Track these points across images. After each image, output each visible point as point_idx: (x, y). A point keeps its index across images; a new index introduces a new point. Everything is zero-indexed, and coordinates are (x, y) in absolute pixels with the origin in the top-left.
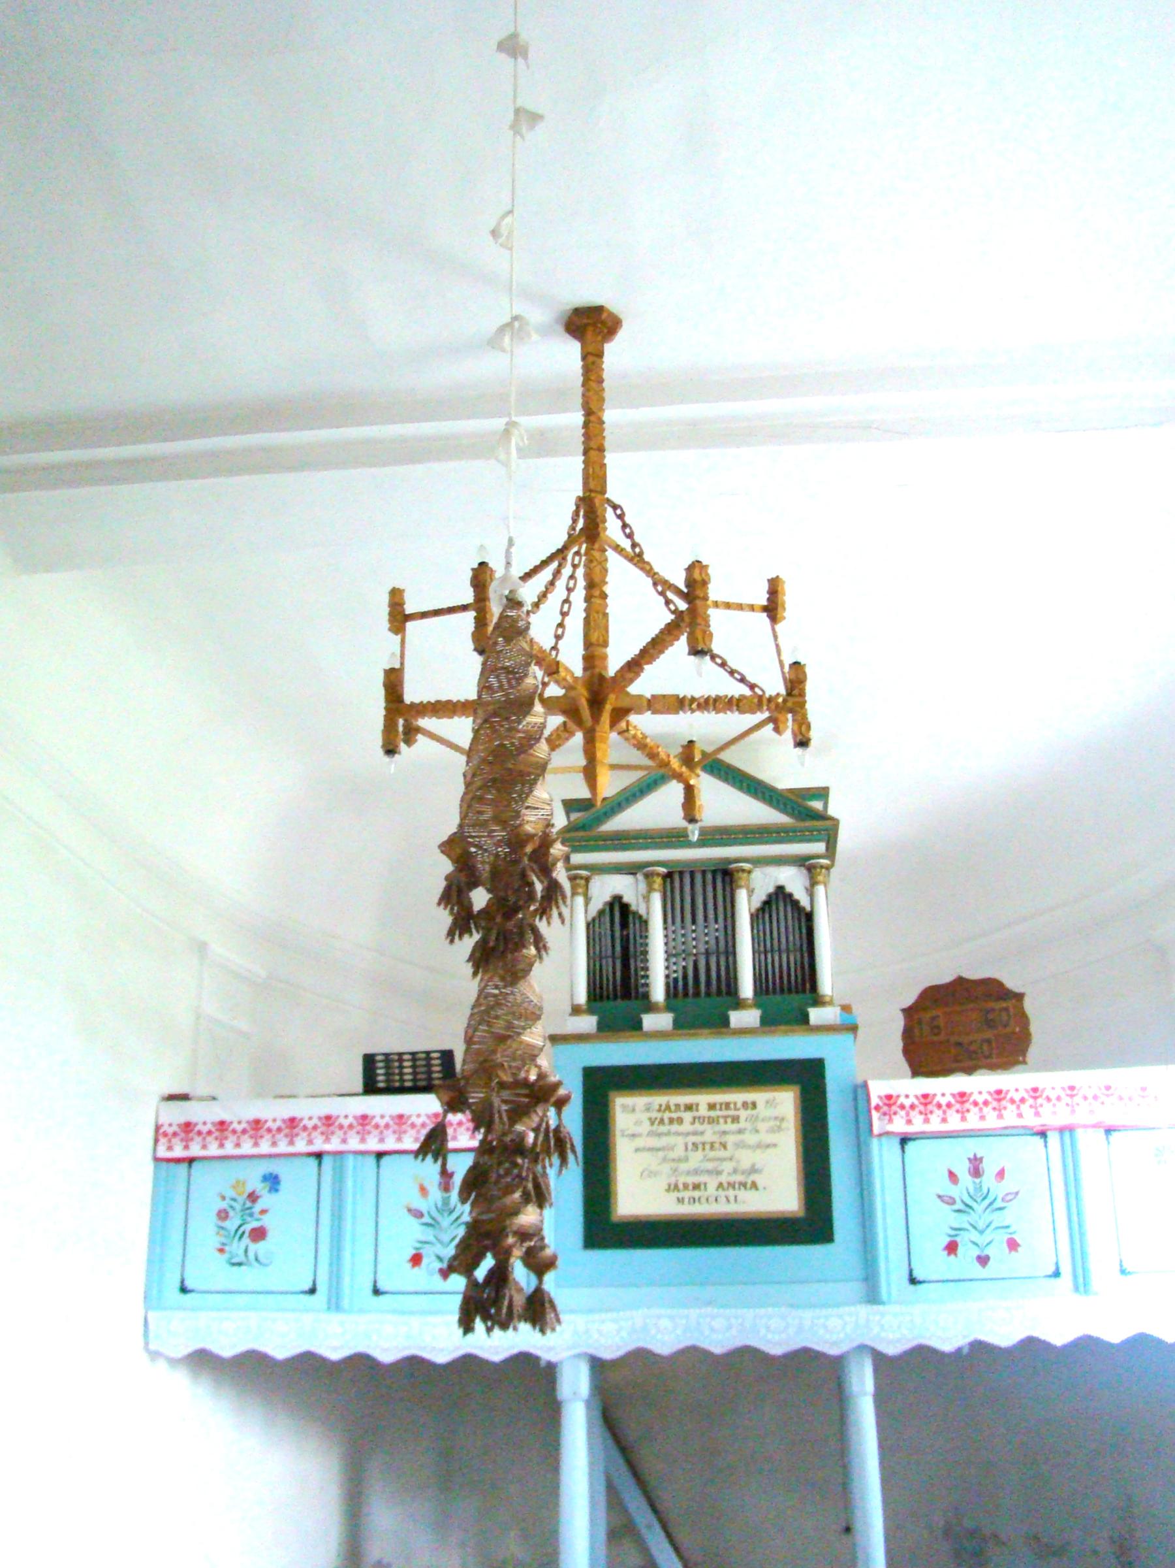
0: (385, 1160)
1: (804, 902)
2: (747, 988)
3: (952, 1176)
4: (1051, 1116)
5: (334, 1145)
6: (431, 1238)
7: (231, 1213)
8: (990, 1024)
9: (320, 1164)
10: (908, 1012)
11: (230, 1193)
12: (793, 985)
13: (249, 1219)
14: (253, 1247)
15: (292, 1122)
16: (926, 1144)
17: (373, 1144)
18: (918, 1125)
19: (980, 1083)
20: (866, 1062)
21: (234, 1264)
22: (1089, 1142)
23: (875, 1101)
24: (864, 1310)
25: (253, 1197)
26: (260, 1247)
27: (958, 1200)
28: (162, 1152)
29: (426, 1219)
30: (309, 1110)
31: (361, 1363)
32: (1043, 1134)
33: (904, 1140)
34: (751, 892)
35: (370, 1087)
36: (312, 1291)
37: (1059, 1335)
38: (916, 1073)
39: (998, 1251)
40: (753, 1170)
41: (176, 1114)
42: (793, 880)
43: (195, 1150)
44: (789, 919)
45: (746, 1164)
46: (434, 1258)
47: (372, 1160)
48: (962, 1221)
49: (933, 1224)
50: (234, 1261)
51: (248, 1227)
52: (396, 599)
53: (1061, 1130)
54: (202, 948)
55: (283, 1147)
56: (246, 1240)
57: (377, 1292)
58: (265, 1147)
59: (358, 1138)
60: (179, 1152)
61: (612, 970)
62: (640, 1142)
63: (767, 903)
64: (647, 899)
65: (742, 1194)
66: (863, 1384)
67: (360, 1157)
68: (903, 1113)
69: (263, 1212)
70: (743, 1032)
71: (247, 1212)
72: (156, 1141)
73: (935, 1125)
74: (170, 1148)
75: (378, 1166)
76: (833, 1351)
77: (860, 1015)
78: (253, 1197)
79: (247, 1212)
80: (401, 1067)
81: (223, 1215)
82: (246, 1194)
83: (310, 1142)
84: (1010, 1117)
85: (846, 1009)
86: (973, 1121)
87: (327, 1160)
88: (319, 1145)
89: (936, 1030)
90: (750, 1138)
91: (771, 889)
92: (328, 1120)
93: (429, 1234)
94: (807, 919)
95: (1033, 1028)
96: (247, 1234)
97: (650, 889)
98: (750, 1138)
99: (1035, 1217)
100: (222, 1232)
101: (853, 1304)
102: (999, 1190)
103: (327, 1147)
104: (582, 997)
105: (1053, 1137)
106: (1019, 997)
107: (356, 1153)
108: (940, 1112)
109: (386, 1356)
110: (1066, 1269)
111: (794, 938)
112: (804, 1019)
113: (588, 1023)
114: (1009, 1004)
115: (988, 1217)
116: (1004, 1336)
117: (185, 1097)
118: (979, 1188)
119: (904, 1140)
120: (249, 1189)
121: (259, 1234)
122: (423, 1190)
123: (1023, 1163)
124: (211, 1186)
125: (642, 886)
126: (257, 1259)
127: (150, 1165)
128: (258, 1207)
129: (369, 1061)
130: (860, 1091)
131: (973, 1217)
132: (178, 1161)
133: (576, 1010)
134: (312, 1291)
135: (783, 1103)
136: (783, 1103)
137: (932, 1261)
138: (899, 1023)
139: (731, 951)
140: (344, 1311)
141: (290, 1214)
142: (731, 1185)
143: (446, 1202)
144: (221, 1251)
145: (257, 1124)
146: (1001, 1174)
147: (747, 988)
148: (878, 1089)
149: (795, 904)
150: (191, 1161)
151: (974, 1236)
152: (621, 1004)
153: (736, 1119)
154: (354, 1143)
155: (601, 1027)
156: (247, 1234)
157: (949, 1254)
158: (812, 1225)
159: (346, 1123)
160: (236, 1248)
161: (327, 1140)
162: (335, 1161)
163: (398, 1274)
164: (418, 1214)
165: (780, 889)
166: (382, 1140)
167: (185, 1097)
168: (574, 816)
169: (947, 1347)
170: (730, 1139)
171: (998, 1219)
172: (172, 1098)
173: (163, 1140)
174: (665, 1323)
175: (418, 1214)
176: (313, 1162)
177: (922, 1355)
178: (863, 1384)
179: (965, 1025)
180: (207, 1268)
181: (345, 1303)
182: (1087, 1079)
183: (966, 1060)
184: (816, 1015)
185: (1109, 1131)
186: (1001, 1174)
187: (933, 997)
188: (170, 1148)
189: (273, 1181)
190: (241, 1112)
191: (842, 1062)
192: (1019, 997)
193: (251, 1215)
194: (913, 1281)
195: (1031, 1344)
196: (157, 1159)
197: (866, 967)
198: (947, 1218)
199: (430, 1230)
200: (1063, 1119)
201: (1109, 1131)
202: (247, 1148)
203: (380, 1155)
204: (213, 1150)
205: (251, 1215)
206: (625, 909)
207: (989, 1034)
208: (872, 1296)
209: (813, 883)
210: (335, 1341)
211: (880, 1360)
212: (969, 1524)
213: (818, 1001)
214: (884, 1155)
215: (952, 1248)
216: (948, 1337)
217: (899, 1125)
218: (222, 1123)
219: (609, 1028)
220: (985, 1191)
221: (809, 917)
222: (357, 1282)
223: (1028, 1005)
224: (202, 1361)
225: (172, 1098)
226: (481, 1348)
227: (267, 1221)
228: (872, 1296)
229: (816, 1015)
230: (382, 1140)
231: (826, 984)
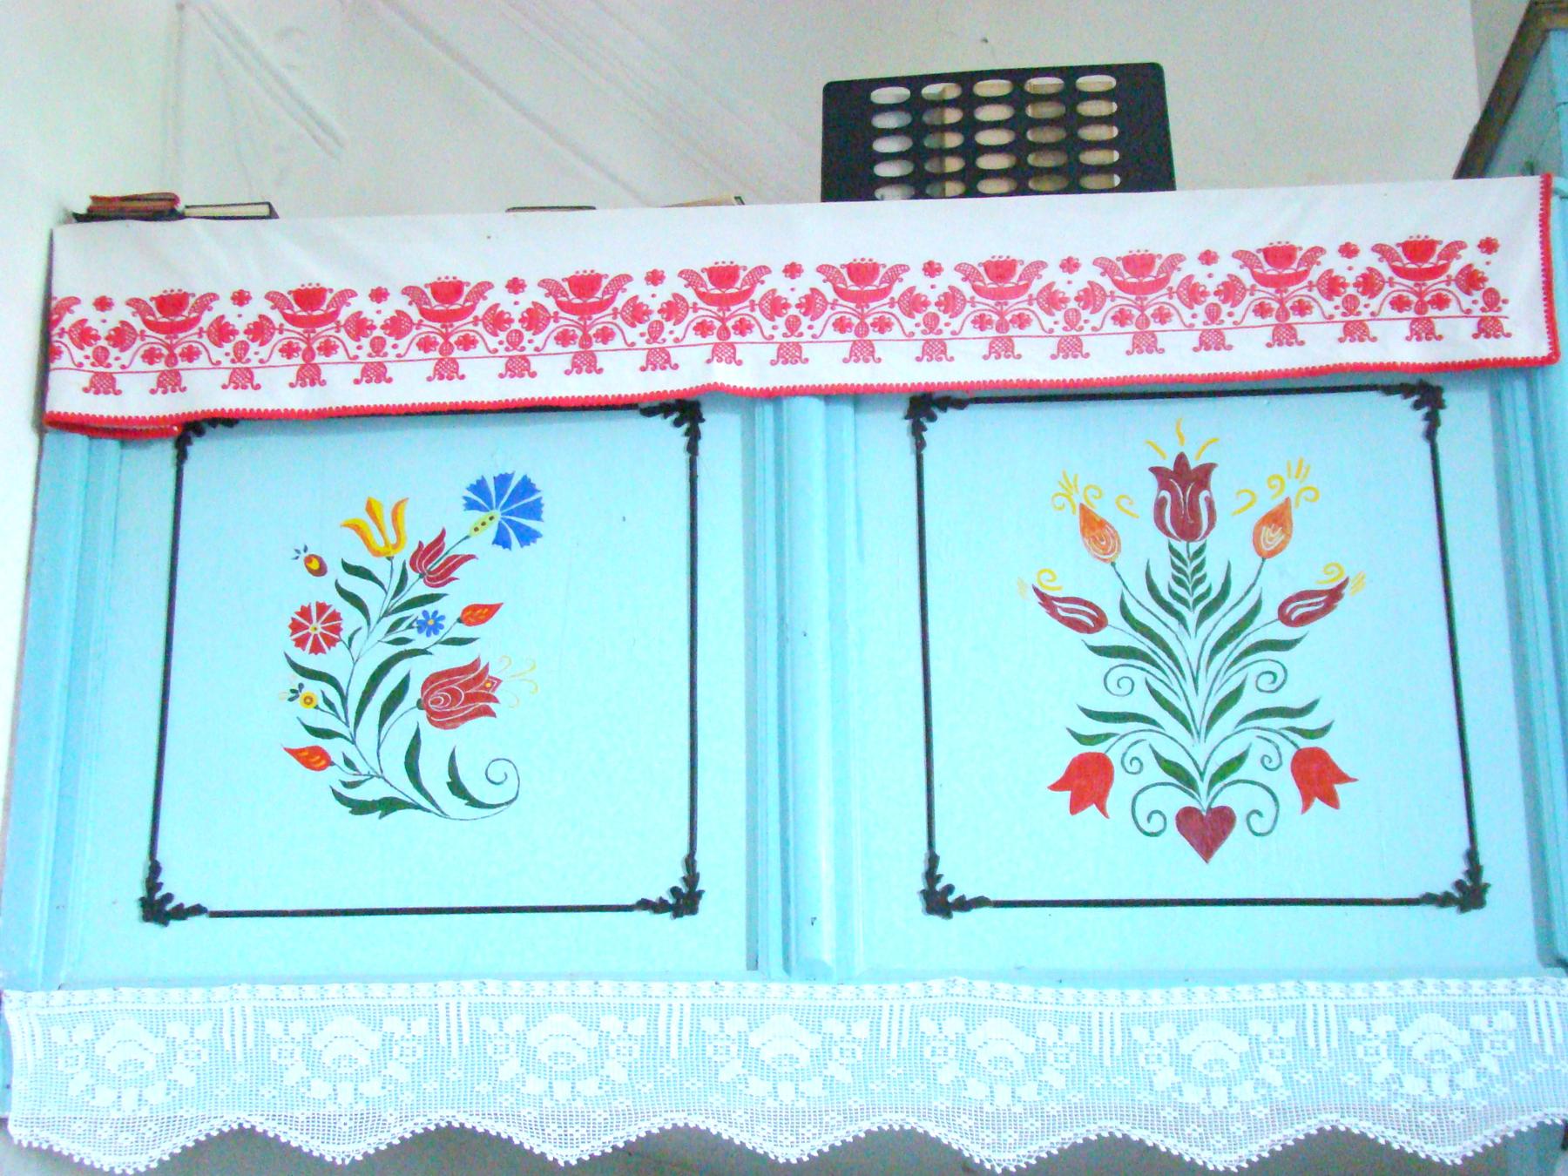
0: (944, 428)
5: (754, 367)
6: (1143, 704)
7: (351, 618)
9: (694, 437)
11: (341, 548)
13: (420, 641)
14: (437, 744)
15: (172, 309)
17: (900, 363)
21: (360, 808)
25: (437, 563)
26: (472, 742)
27: (1113, 616)
28: (70, 396)
29: (1116, 634)
30: (649, 245)
32: (1424, 390)
35: (847, 175)
36: (685, 901)
41: (128, 267)
43: (206, 389)
46: (1155, 773)
47: (893, 425)
50: (371, 791)
51: (419, 670)
55: (552, 377)
56: (410, 717)
57: (939, 901)
58: (483, 380)
59: (289, 370)
60: (137, 397)
67: (846, 411)
68: (634, 334)
69: (478, 614)
71: (412, 613)
72: (48, 353)
74: (103, 384)
75: (920, 445)
78: (437, 563)
79: (412, 613)
80: (970, 126)
81: (315, 629)
82: (405, 554)
83: (659, 359)
87: (719, 428)
88: (692, 368)
91: (102, 396)
96: (414, 693)
100: (314, 687)
101: (1513, 973)
103: (724, 374)
107: (830, 395)
108: (1055, 321)
117: (162, 209)
118: (1188, 571)
120: (420, 533)
121: (464, 695)
122: (1094, 528)
124: (269, 522)
126: (457, 787)
127: (28, 439)
128: (451, 605)
129: (847, 107)
132: (128, 432)
134: (685, 901)
140: (815, 973)
141: (591, 603)
143: (1188, 571)
144: (313, 759)
145: (447, 300)
154: (827, 361)
156: (414, 693)
157: (1331, 800)
159: (794, 292)
160: (377, 749)
161: (725, 352)
162: (1496, 399)
163: (1009, 830)
166: (935, 350)
167: (162, 209)
172: (102, 211)
174: (1432, 1033)
176: (667, 434)
180: (255, 822)
181: (822, 943)
188: (103, 384)
189: (514, 507)
190: (380, 259)
193: (431, 625)
194: (939, 901)
196: (50, 423)
199: (1136, 673)
202: (412, 381)
203: (924, 405)
205: (431, 625)
218: (309, 297)
220: (1214, 580)
225: (102, 211)
226: (1381, 1113)
227: (489, 647)
230: (935, 350)
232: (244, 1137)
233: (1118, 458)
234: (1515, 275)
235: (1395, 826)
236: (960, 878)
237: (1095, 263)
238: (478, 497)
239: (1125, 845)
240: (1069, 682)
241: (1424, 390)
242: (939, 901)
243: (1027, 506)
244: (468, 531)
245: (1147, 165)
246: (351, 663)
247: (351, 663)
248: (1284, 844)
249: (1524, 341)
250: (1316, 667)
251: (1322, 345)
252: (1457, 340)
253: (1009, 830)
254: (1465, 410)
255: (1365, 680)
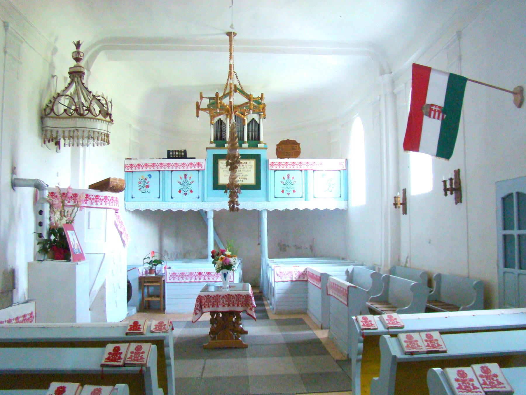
1: (258, 122)
2: (246, 139)
3: (284, 178)
4: (303, 167)
8: (293, 149)
10: (277, 145)
12: (255, 139)
16: (280, 173)
17: (171, 169)
18: (278, 168)
19: (290, 160)
20: (267, 150)
22: (310, 173)
23: (270, 163)
24: (266, 202)
25: (146, 179)
26: (148, 189)
28: (126, 170)
31: (159, 211)
32: (301, 171)
33: (275, 171)
34: (247, 119)
35: (169, 157)
36: (159, 198)
37: (301, 208)
38: (278, 158)
39: (291, 193)
40: (246, 176)
41: (128, 162)
42: (256, 117)
43: (134, 170)
44: (255, 126)
45: (245, 175)
48: (285, 186)
49: (280, 187)
52: (201, 94)
53: (305, 170)
54: (130, 126)
55: (152, 169)
58: (148, 169)
60: (130, 170)
61: (218, 134)
62: (224, 170)
63: (251, 122)
64: (226, 119)
65: (244, 180)
66: (265, 216)
70: (244, 148)
73: (281, 168)
76: (260, 210)
77: (268, 147)
78: (146, 179)
81: (140, 183)
84: (295, 167)
85: (265, 144)
86: (288, 168)
87: (161, 172)
89: (282, 149)
90: (246, 169)
92: (161, 164)
93: (182, 187)
94: (258, 126)
95: (301, 150)
97: (227, 118)
98: (246, 169)
99: (298, 187)
102: (292, 181)
104: (212, 140)
105: (303, 171)
106: (299, 144)
109: (281, 209)
110: (304, 196)
111: (256, 129)
112: (257, 146)
113: (214, 145)
114: (297, 145)
115: (290, 186)
116: (291, 208)
117: (130, 159)
118: (185, 180)
119: (275, 171)
121: (148, 187)
122: (181, 178)
123: (297, 176)
125: (225, 117)
129: (169, 151)
130: (267, 161)
131: (287, 186)
133: (211, 142)
135: (253, 162)
136: (253, 162)
137: (279, 194)
138: (276, 147)
139: (243, 131)
141: (154, 182)
142: (242, 178)
143: (185, 180)
145: (146, 164)
146: (293, 178)
147: (246, 139)
148: (271, 161)
149: (256, 122)
150: (132, 172)
151: (287, 189)
152: (220, 141)
153: (243, 166)
154: (167, 169)
155: (217, 146)
158: (257, 186)
160: (143, 189)
161: (217, 278)
163: (176, 194)
164: (180, 183)
165: (253, 119)
167: (130, 159)
168: (211, 101)
169: (281, 210)
170: (242, 169)
171: (292, 186)
172: (127, 159)
173: (126, 168)
175: (180, 183)
177: (276, 211)
178: (265, 216)
179: (288, 149)
182: (311, 161)
183: (288, 156)
184: (259, 145)
185: (314, 171)
186: (293, 178)
187: (282, 143)
189: (150, 176)
191: (264, 155)
192: (299, 144)
194: (275, 197)
195: (296, 210)
197: (270, 135)
198: (282, 186)
200: (306, 168)
201: (314, 171)
202: (144, 169)
203: (172, 171)
204: (137, 170)
206: (221, 121)
207: (293, 151)
208: (267, 200)
209: (260, 118)
210: (164, 206)
211: (268, 212)
212: (283, 243)
213: (260, 143)
214: (271, 174)
215: (283, 191)
216: (281, 207)
217: (274, 168)
219: (218, 146)
221: (259, 125)
222: (168, 196)
223: (301, 146)
224: (137, 212)
225: (127, 159)
227: (149, 184)
228: (267, 200)
229: (259, 145)
231: (262, 139)
232: (147, 210)
233: (182, 174)
234: (203, 165)
235: (195, 194)
236: (173, 197)
237: (457, 173)
238: (148, 175)
239: (182, 195)
240: (179, 186)
241: (198, 171)
242: (172, 198)
243: (177, 177)
244: (148, 177)
245: (185, 157)
246: (142, 185)
247: (142, 185)
248: (190, 195)
249: (203, 169)
250: (192, 186)
251: (193, 168)
252: (200, 168)
253: (176, 194)
254: (200, 172)
255: (194, 187)
